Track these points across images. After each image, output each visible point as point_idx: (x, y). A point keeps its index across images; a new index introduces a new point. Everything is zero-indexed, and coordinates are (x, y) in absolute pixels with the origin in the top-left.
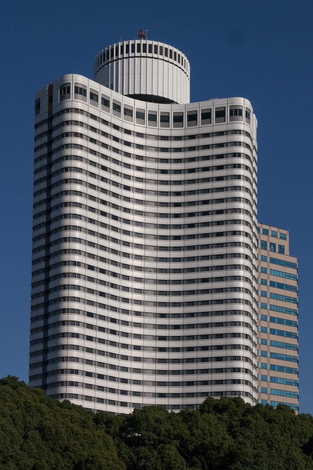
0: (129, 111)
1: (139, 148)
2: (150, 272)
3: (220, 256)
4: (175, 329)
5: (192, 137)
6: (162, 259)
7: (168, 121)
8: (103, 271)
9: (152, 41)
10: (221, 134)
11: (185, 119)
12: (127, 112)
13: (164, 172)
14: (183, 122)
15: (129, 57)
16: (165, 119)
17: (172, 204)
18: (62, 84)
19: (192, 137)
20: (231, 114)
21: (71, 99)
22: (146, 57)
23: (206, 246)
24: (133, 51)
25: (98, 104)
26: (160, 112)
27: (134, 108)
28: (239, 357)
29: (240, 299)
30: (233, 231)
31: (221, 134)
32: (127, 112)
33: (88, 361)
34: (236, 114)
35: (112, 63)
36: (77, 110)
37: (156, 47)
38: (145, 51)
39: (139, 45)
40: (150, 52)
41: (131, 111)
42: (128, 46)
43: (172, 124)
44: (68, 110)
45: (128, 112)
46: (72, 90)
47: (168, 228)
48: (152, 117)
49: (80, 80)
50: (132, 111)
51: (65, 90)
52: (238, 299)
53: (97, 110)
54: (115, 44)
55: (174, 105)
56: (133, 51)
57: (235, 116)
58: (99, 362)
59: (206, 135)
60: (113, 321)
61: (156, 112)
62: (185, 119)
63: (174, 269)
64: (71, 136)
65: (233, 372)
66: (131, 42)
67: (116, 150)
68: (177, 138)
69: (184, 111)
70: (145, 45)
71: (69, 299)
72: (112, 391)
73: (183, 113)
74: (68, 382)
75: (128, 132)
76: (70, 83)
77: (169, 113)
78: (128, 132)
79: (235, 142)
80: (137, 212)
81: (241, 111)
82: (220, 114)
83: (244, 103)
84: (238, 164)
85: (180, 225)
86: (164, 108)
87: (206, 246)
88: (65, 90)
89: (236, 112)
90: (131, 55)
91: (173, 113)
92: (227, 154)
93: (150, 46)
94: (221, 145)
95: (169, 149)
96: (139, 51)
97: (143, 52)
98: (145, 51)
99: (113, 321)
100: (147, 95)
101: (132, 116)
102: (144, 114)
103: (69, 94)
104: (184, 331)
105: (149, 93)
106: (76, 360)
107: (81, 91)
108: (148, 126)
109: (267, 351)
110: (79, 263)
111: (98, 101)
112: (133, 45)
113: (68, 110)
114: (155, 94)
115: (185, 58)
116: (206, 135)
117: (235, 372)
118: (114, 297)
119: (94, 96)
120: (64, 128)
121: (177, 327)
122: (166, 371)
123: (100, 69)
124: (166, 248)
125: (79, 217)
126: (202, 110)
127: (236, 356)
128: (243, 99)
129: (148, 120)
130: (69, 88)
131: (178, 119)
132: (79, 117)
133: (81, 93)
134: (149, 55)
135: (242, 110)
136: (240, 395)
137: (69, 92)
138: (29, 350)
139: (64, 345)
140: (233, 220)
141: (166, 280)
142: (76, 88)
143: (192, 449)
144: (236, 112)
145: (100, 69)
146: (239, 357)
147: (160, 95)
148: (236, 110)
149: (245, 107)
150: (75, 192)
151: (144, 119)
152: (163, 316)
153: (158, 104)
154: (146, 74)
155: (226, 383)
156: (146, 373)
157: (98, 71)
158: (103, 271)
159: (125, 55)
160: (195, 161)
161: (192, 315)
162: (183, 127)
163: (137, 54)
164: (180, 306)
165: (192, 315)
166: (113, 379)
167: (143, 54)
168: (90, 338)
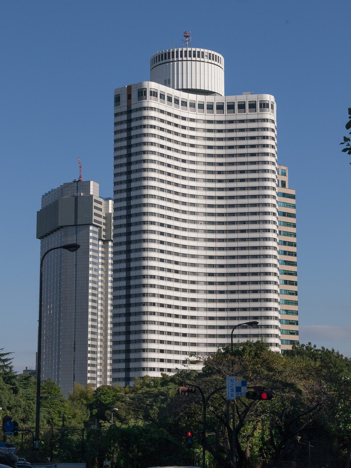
0: (184, 102)
1: (192, 163)
2: (201, 224)
3: (254, 180)
4: (220, 267)
5: (231, 122)
6: (209, 214)
7: (212, 109)
8: (169, 149)
9: (199, 49)
10: (253, 121)
11: (225, 107)
12: (183, 103)
13: (211, 318)
14: (223, 109)
15: (183, 61)
16: (210, 107)
17: (216, 122)
18: (140, 88)
19: (231, 122)
20: (261, 107)
21: (147, 100)
22: (196, 61)
23: (243, 189)
24: (186, 56)
25: (165, 101)
26: (206, 102)
28: (270, 291)
29: (269, 195)
30: (263, 144)
31: (253, 121)
32: (183, 103)
33: (161, 268)
34: (264, 107)
35: (173, 63)
36: (152, 109)
37: (203, 53)
38: (194, 56)
39: (190, 52)
40: (199, 57)
41: (186, 103)
42: (181, 52)
43: (216, 111)
44: (145, 108)
45: (184, 103)
46: (148, 93)
47: (214, 250)
48: (201, 106)
49: (153, 86)
50: (187, 102)
51: (142, 93)
52: (267, 178)
53: (165, 106)
54: (175, 49)
55: (217, 97)
56: (186, 56)
57: (264, 108)
58: (168, 233)
59: (242, 121)
60: (177, 263)
61: (204, 102)
62: (225, 107)
63: (220, 300)
64: (148, 127)
65: (266, 310)
66: (184, 49)
67: (177, 134)
68: (219, 122)
70: (194, 52)
71: (148, 267)
72: (177, 202)
73: (223, 103)
74: (148, 368)
75: (184, 119)
76: (146, 88)
77: (213, 103)
78: (184, 119)
79: (264, 119)
80: (191, 178)
81: (268, 104)
82: (253, 106)
83: (269, 98)
84: (266, 136)
85: (222, 146)
86: (209, 99)
87: (243, 189)
88: (142, 93)
89: (264, 105)
90: (184, 59)
91: (216, 103)
92: (259, 195)
93: (199, 52)
94: (253, 130)
95: (213, 138)
96: (190, 56)
97: (193, 57)
98: (194, 56)
99: (177, 263)
100: (196, 89)
101: (186, 106)
102: (195, 104)
103: (145, 96)
105: (198, 88)
106: (154, 188)
107: (154, 94)
108: (198, 113)
109: (295, 204)
110: (154, 223)
111: (164, 99)
112: (186, 52)
113: (145, 108)
114: (202, 88)
116: (242, 121)
117: (268, 310)
118: (177, 176)
119: (162, 96)
120: (142, 121)
121: (221, 266)
122: (213, 222)
124: (212, 223)
125: (154, 135)
126: (238, 102)
127: (268, 290)
128: (269, 95)
129: (198, 108)
130: (145, 92)
131: (220, 107)
132: (152, 113)
133: (154, 96)
134: (198, 59)
135: (269, 104)
137: (145, 94)
139: (145, 133)
140: (263, 128)
141: (213, 230)
142: (151, 92)
144: (264, 105)
146: (270, 291)
147: (206, 89)
148: (264, 104)
149: (271, 101)
150: (151, 169)
151: (195, 108)
152: (211, 257)
153: (205, 96)
154: (196, 73)
155: (260, 275)
156: (199, 301)
158: (169, 149)
159: (180, 59)
160: (234, 198)
161: (233, 257)
162: (224, 114)
163: (189, 59)
164: (224, 250)
165: (233, 257)
166: (177, 176)
167: (193, 59)
168: (162, 146)
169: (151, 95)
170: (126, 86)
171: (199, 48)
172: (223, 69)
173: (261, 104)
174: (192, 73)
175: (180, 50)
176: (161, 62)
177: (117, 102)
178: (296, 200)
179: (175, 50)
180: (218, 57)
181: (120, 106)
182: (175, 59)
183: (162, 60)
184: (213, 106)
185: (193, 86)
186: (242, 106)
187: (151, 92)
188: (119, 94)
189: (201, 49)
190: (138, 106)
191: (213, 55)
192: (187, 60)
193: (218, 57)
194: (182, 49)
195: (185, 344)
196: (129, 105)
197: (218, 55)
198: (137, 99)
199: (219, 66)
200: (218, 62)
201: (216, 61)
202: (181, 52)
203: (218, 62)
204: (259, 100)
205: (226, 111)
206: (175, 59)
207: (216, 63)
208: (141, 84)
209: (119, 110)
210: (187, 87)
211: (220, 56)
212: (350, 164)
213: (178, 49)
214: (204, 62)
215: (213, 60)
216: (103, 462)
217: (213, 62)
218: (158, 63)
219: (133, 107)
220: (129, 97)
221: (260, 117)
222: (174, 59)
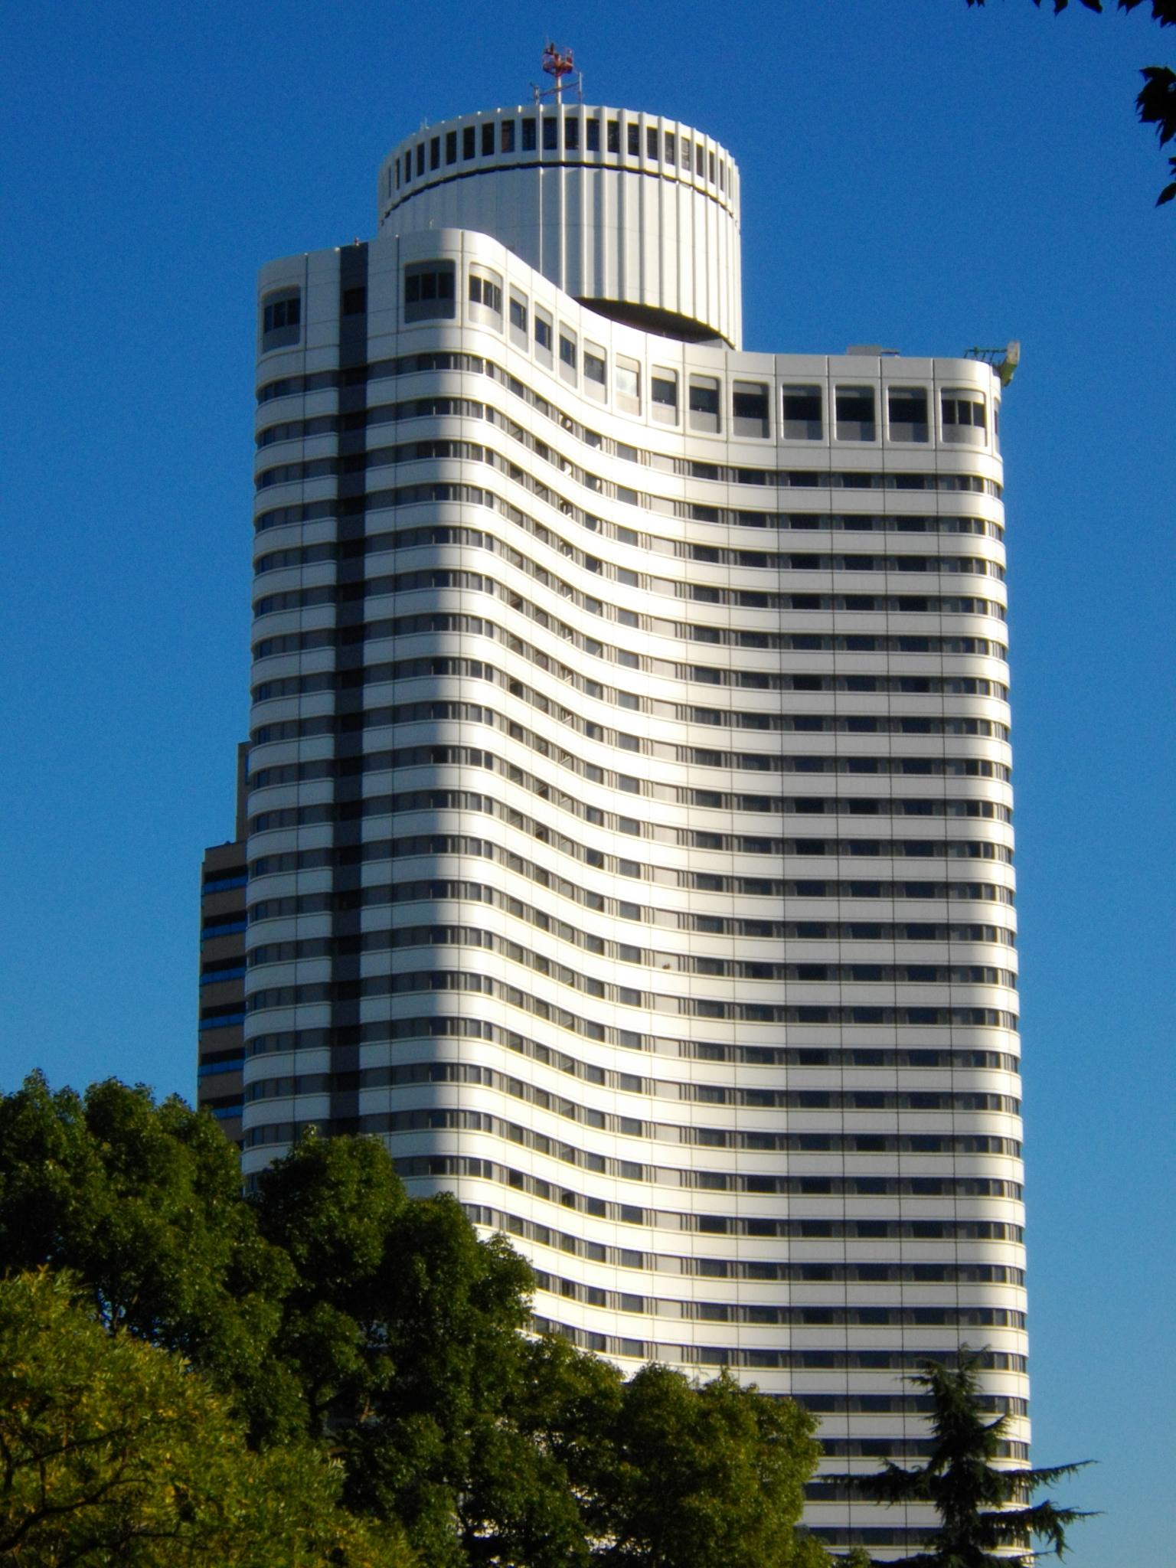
2: (666, 967)
8: (542, 616)
20: (948, 419)
27: (684, 376)
34: (965, 420)
37: (671, 138)
39: (634, 129)
46: (462, 289)
69: (721, 376)
90: (609, 158)
96: (635, 150)
104: (961, 1332)
107: (486, 293)
112: (614, 127)
114: (670, 306)
115: (722, 154)
123: (396, 207)
136: (574, 1343)
138: (199, 955)
143: (322, 1309)
145: (396, 207)
147: (687, 312)
148: (965, 406)
153: (774, 356)
157: (388, 214)
159: (587, 156)
169: (475, 296)
170: (337, 249)
171: (654, 114)
172: (737, 215)
173: (948, 406)
175: (586, 112)
179: (564, 111)
180: (712, 155)
181: (300, 346)
182: (563, 155)
187: (475, 282)
188: (297, 289)
189: (681, 125)
190: (413, 343)
192: (640, 172)
194: (598, 113)
198: (402, 311)
202: (594, 125)
205: (782, 427)
206: (563, 155)
208: (435, 238)
209: (286, 364)
212: (1063, 12)
213: (578, 111)
214: (657, 176)
216: (912, 1558)
219: (378, 351)
222: (558, 155)
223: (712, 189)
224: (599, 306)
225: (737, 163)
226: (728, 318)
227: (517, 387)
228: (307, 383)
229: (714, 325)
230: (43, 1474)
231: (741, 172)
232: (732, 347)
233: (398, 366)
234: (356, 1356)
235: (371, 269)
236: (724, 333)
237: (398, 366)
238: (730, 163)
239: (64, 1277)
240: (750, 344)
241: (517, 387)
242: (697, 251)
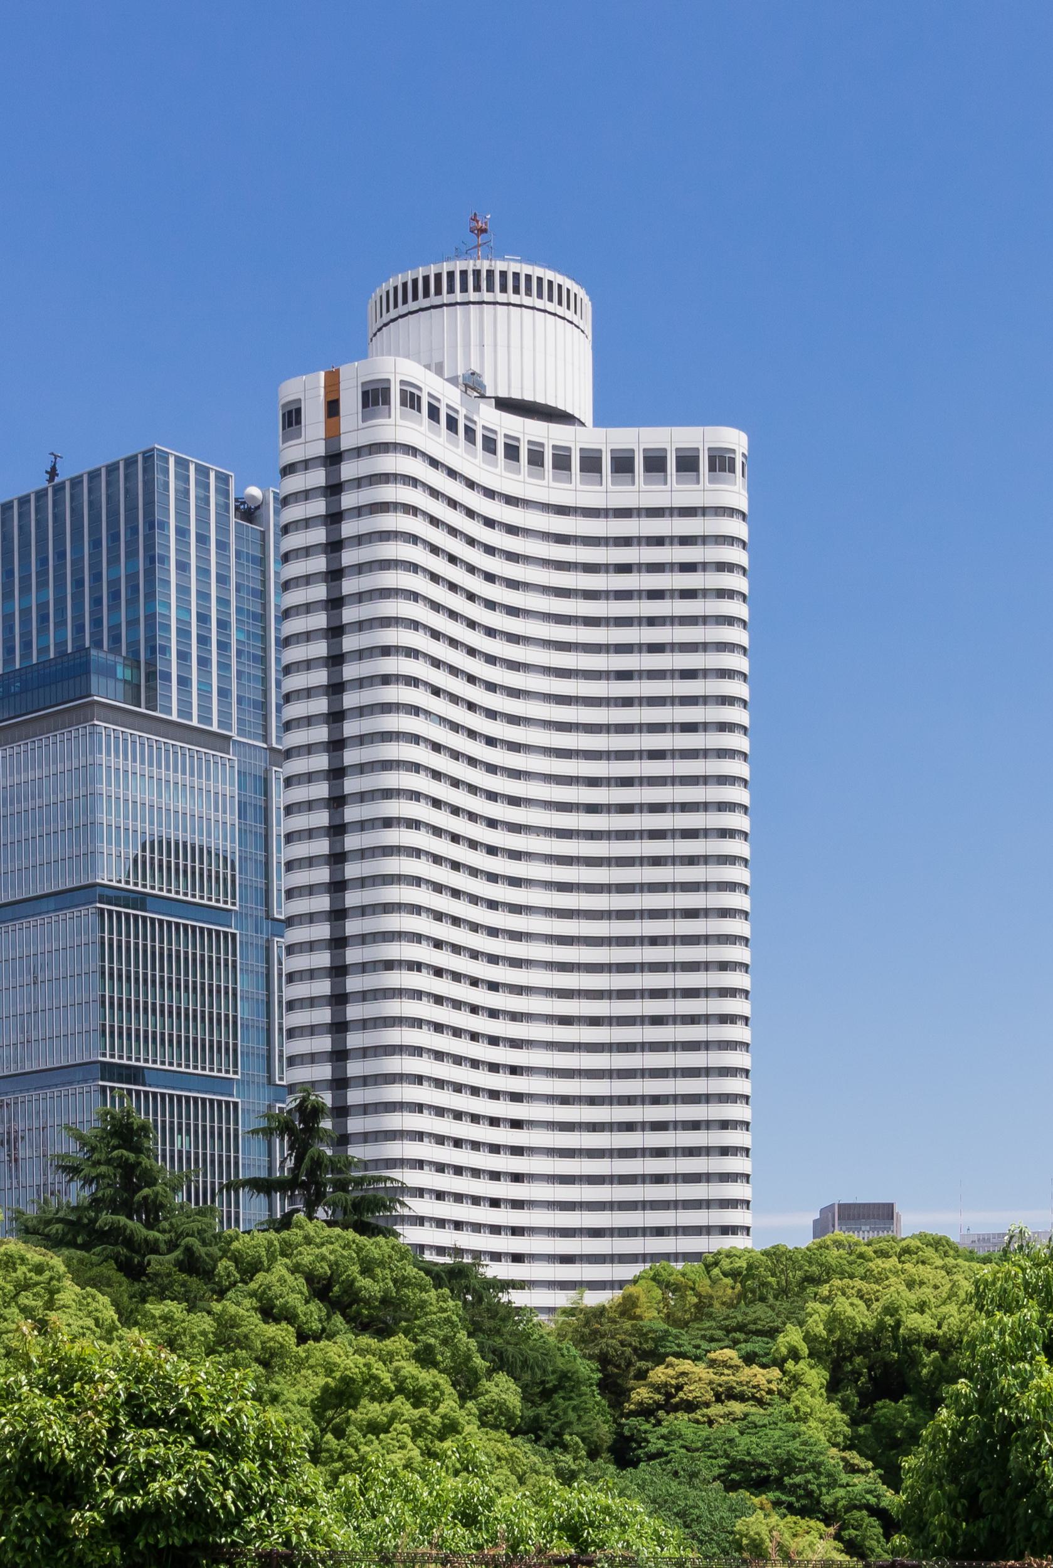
83: (735, 440)
172: (590, 337)
173: (712, 460)
174: (509, 347)
176: (412, 306)
177: (290, 425)
178: (752, 1083)
181: (302, 440)
183: (415, 298)
184: (696, 459)
185: (512, 390)
186: (655, 463)
188: (299, 400)
190: (363, 439)
191: (540, 280)
193: (568, 290)
195: (496, 1230)
196: (333, 435)
197: (575, 288)
199: (560, 317)
200: (568, 308)
201: (550, 299)
203: (568, 308)
204: (707, 446)
207: (561, 311)
209: (294, 452)
210: (509, 392)
211: (582, 293)
215: (527, 294)
217: (539, 304)
218: (402, 309)
219: (347, 442)
220: (333, 408)
221: (710, 501)
223: (569, 315)
224: (506, 405)
225: (591, 300)
226: (581, 403)
227: (434, 463)
228: (306, 464)
229: (570, 411)
230: (806, 1386)
231: (593, 306)
232: (583, 424)
233: (359, 452)
234: (354, 1280)
235: (342, 386)
236: (577, 415)
237: (359, 452)
238: (586, 299)
239: (247, 1190)
240: (596, 424)
241: (434, 463)
242: (512, 349)
